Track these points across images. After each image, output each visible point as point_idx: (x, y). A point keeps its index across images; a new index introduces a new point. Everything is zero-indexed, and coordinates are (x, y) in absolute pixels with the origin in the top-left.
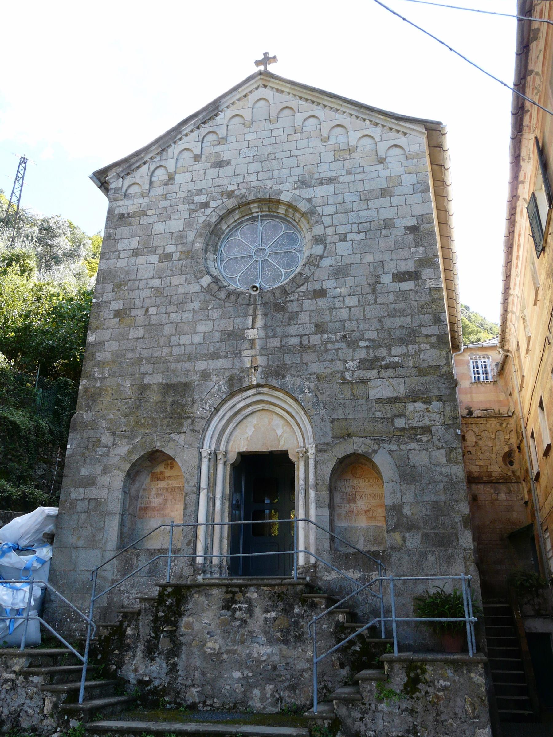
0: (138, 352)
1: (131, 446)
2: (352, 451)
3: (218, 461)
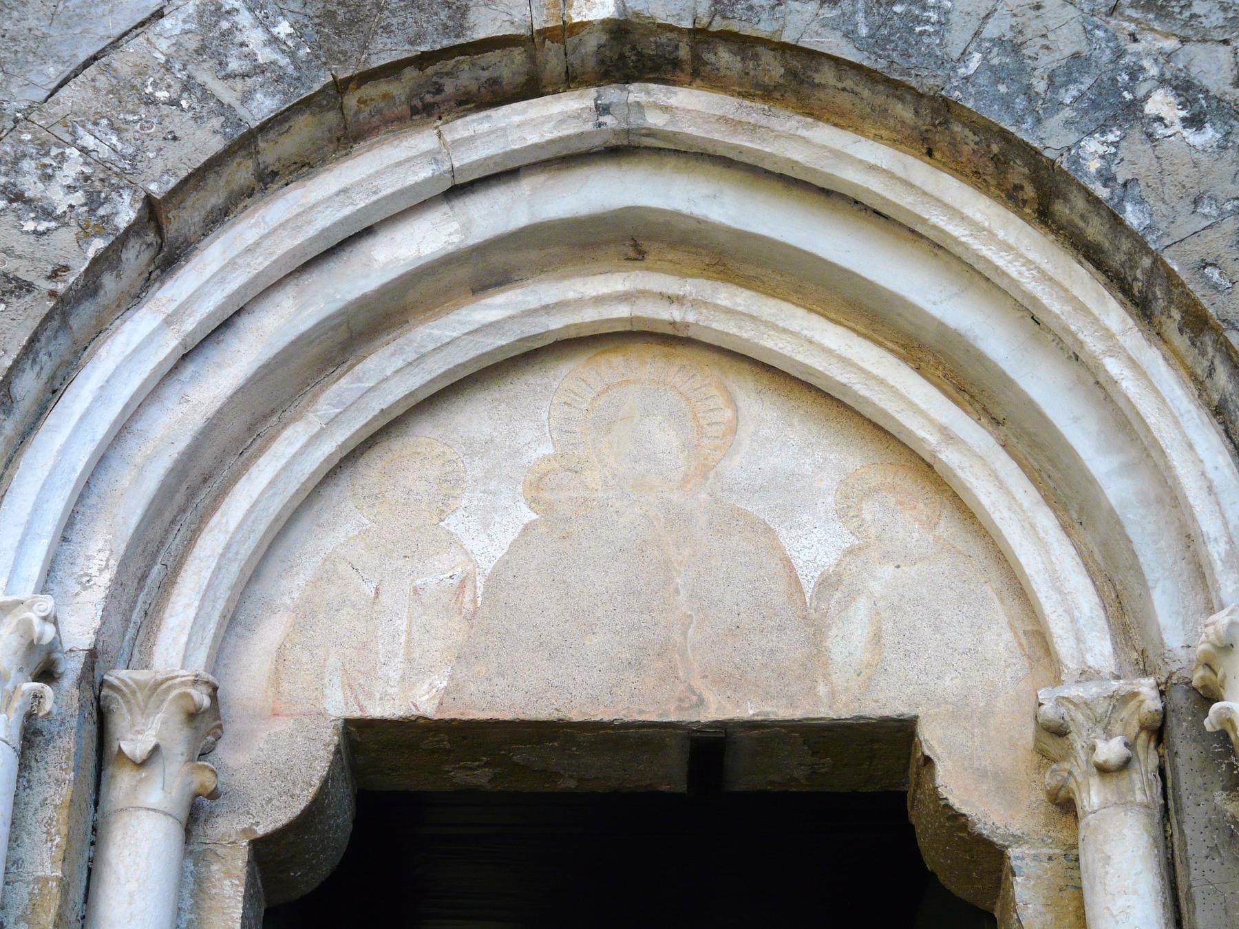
3: (122, 783)
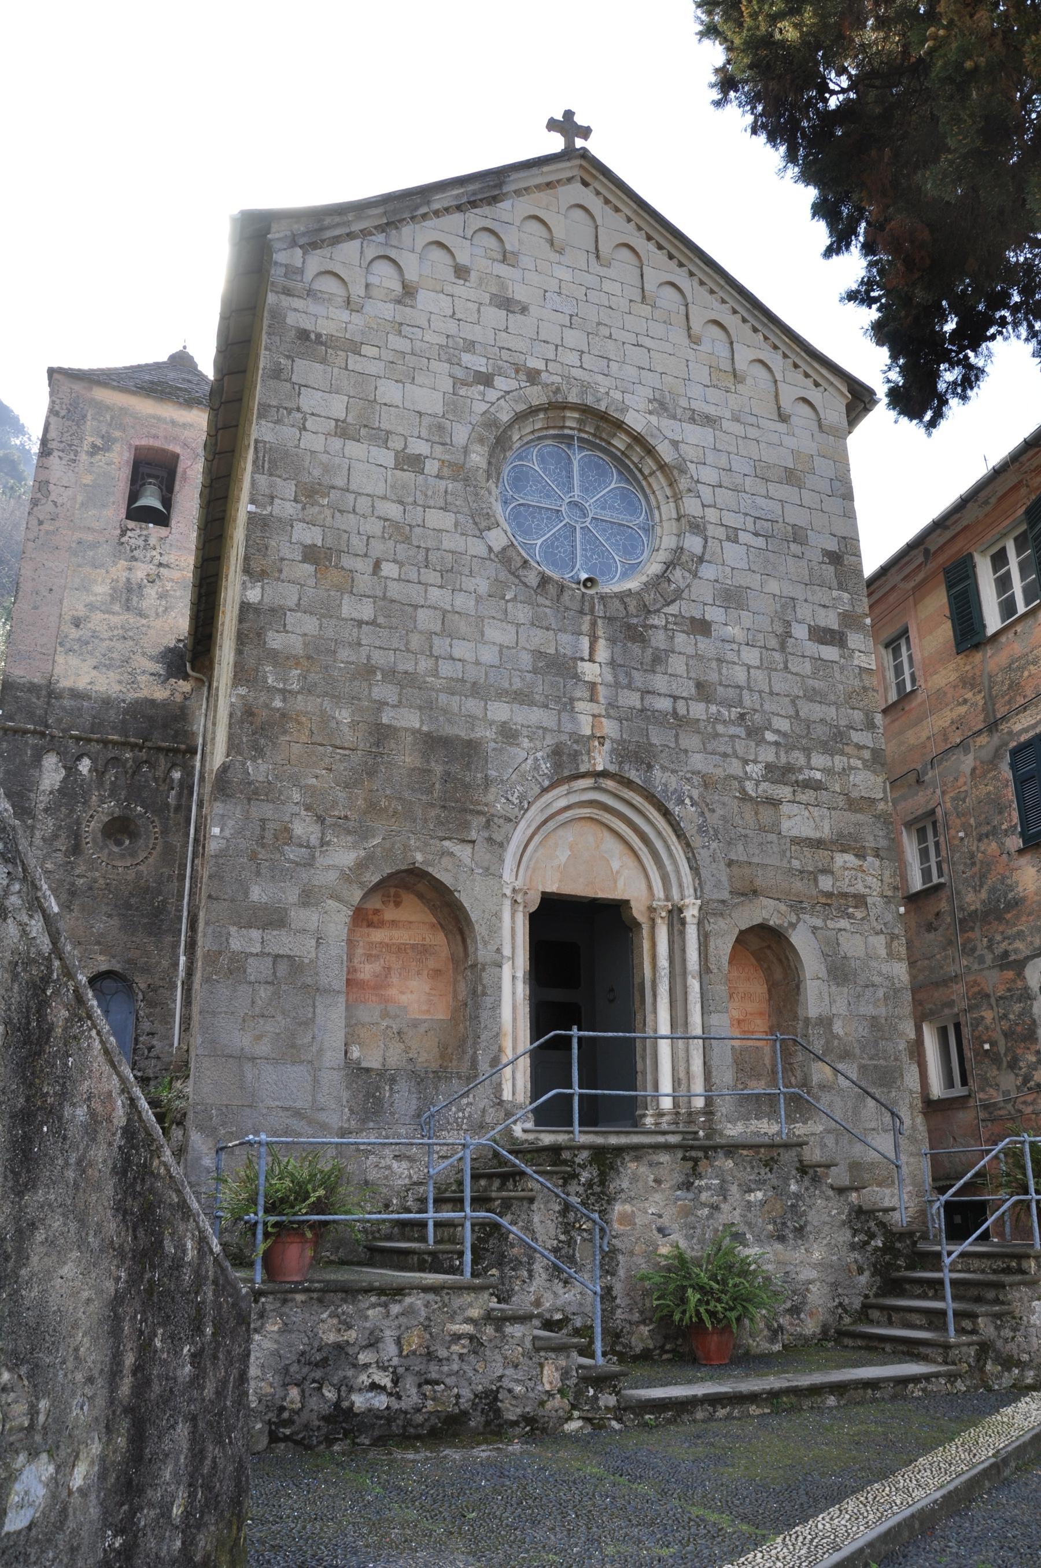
0: (364, 651)
1: (362, 853)
2: (759, 921)
